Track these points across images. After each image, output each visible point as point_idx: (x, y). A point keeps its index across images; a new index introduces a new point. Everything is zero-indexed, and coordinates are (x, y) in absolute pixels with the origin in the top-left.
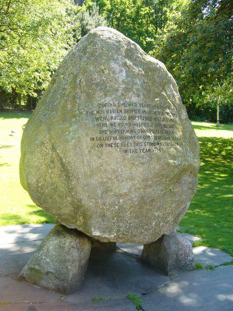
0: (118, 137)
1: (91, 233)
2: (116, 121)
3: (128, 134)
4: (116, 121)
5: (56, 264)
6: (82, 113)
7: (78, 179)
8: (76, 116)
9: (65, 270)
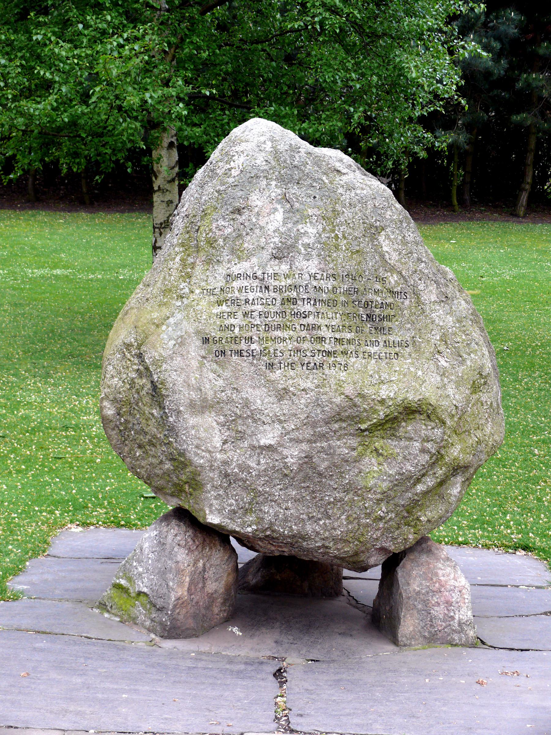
0: (255, 338)
1: (205, 518)
2: (253, 308)
3: (308, 308)
4: (253, 308)
5: (153, 577)
6: (193, 292)
7: (179, 412)
8: (183, 297)
9: (165, 590)
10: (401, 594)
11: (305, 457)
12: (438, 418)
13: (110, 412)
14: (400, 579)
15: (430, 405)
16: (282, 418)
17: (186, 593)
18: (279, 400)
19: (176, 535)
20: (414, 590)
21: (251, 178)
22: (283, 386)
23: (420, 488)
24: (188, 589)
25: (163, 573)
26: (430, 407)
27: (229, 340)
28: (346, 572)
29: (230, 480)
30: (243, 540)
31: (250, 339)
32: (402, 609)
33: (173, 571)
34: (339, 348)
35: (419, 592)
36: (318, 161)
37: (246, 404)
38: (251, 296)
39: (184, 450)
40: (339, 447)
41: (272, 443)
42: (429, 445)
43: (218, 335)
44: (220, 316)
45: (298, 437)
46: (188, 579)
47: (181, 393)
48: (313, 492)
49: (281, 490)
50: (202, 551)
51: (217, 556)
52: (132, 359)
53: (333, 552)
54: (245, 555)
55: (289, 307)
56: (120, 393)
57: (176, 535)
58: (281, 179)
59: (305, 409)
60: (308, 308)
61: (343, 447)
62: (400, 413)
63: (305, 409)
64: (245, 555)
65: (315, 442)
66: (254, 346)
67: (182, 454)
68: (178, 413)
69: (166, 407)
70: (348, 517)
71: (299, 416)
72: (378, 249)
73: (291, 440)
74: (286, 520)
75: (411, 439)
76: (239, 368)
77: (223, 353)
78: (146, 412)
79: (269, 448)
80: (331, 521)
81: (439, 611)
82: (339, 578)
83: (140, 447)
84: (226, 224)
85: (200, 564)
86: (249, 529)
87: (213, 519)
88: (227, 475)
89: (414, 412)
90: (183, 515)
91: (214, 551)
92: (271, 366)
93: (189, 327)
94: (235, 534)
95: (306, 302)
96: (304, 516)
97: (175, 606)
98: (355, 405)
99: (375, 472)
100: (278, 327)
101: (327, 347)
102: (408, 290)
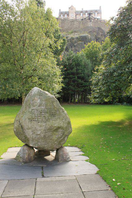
3: (44, 113)
13: (15, 130)
21: (35, 95)
23: (61, 139)
25: (24, 154)
28: (51, 152)
30: (36, 148)
31: (35, 119)
34: (48, 119)
36: (44, 93)
38: (35, 112)
44: (31, 115)
47: (25, 127)
51: (32, 151)
53: (49, 149)
54: (36, 150)
55: (41, 114)
58: (39, 95)
60: (44, 113)
61: (50, 134)
64: (36, 150)
67: (26, 136)
72: (53, 105)
74: (42, 145)
77: (32, 121)
79: (39, 134)
81: (65, 157)
82: (50, 153)
87: (31, 145)
89: (60, 128)
90: (26, 145)
92: (39, 122)
93: (26, 117)
94: (34, 147)
99: (55, 137)
100: (39, 117)
101: (47, 119)
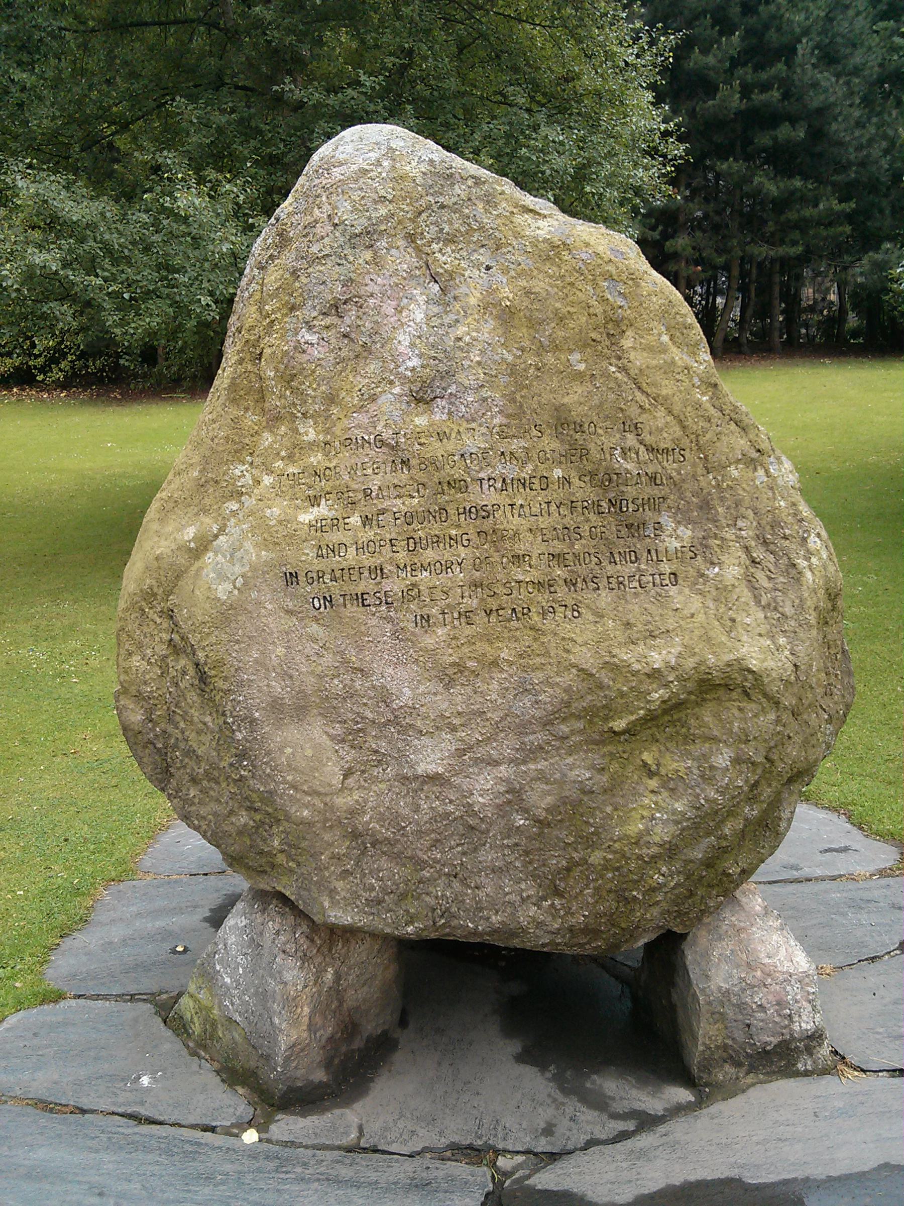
7: (253, 721)
10: (695, 995)
11: (507, 792)
12: (765, 695)
14: (690, 968)
15: (750, 671)
16: (456, 721)
17: (305, 1035)
18: (447, 687)
19: (278, 933)
20: (720, 988)
22: (455, 658)
24: (310, 1025)
26: (750, 677)
27: (338, 574)
29: (364, 843)
32: (699, 1022)
33: (278, 997)
35: (728, 991)
37: (384, 697)
39: (270, 792)
40: (572, 767)
41: (440, 770)
42: (749, 751)
43: (318, 565)
45: (490, 755)
46: (306, 1010)
48: (527, 853)
49: (464, 854)
50: (330, 950)
52: (159, 621)
56: (145, 683)
57: (278, 933)
59: (500, 701)
62: (690, 693)
63: (500, 701)
65: (524, 762)
66: (387, 585)
68: (251, 722)
69: (228, 713)
70: (597, 889)
71: (489, 715)
73: (477, 761)
75: (715, 740)
76: (363, 628)
78: (195, 718)
79: (434, 778)
80: (564, 901)
83: (194, 780)
84: (313, 338)
85: (329, 975)
86: (410, 929)
88: (355, 835)
91: (354, 942)
95: (485, 486)
96: (513, 897)
97: (287, 1059)
98: (601, 687)
102: (685, 442)
